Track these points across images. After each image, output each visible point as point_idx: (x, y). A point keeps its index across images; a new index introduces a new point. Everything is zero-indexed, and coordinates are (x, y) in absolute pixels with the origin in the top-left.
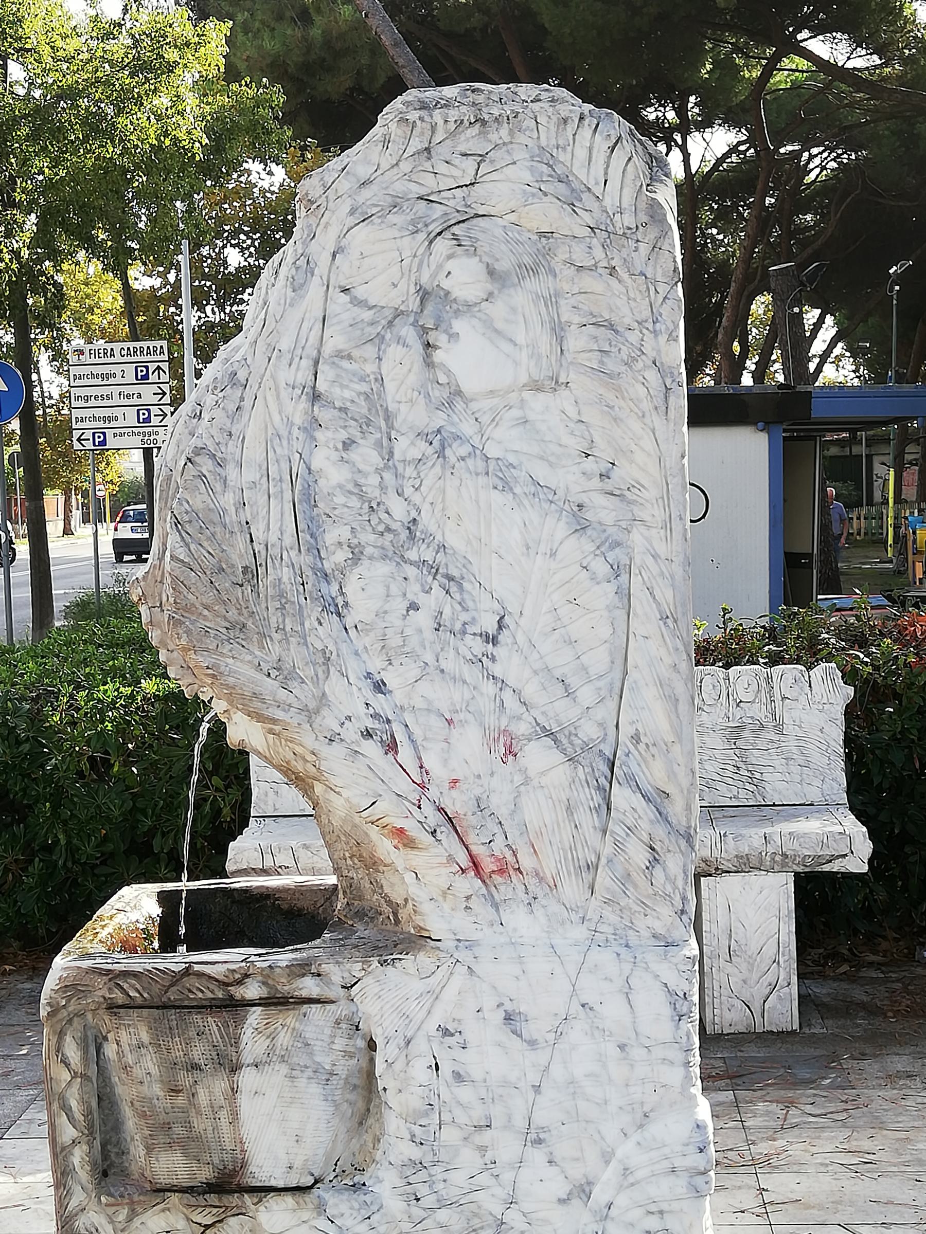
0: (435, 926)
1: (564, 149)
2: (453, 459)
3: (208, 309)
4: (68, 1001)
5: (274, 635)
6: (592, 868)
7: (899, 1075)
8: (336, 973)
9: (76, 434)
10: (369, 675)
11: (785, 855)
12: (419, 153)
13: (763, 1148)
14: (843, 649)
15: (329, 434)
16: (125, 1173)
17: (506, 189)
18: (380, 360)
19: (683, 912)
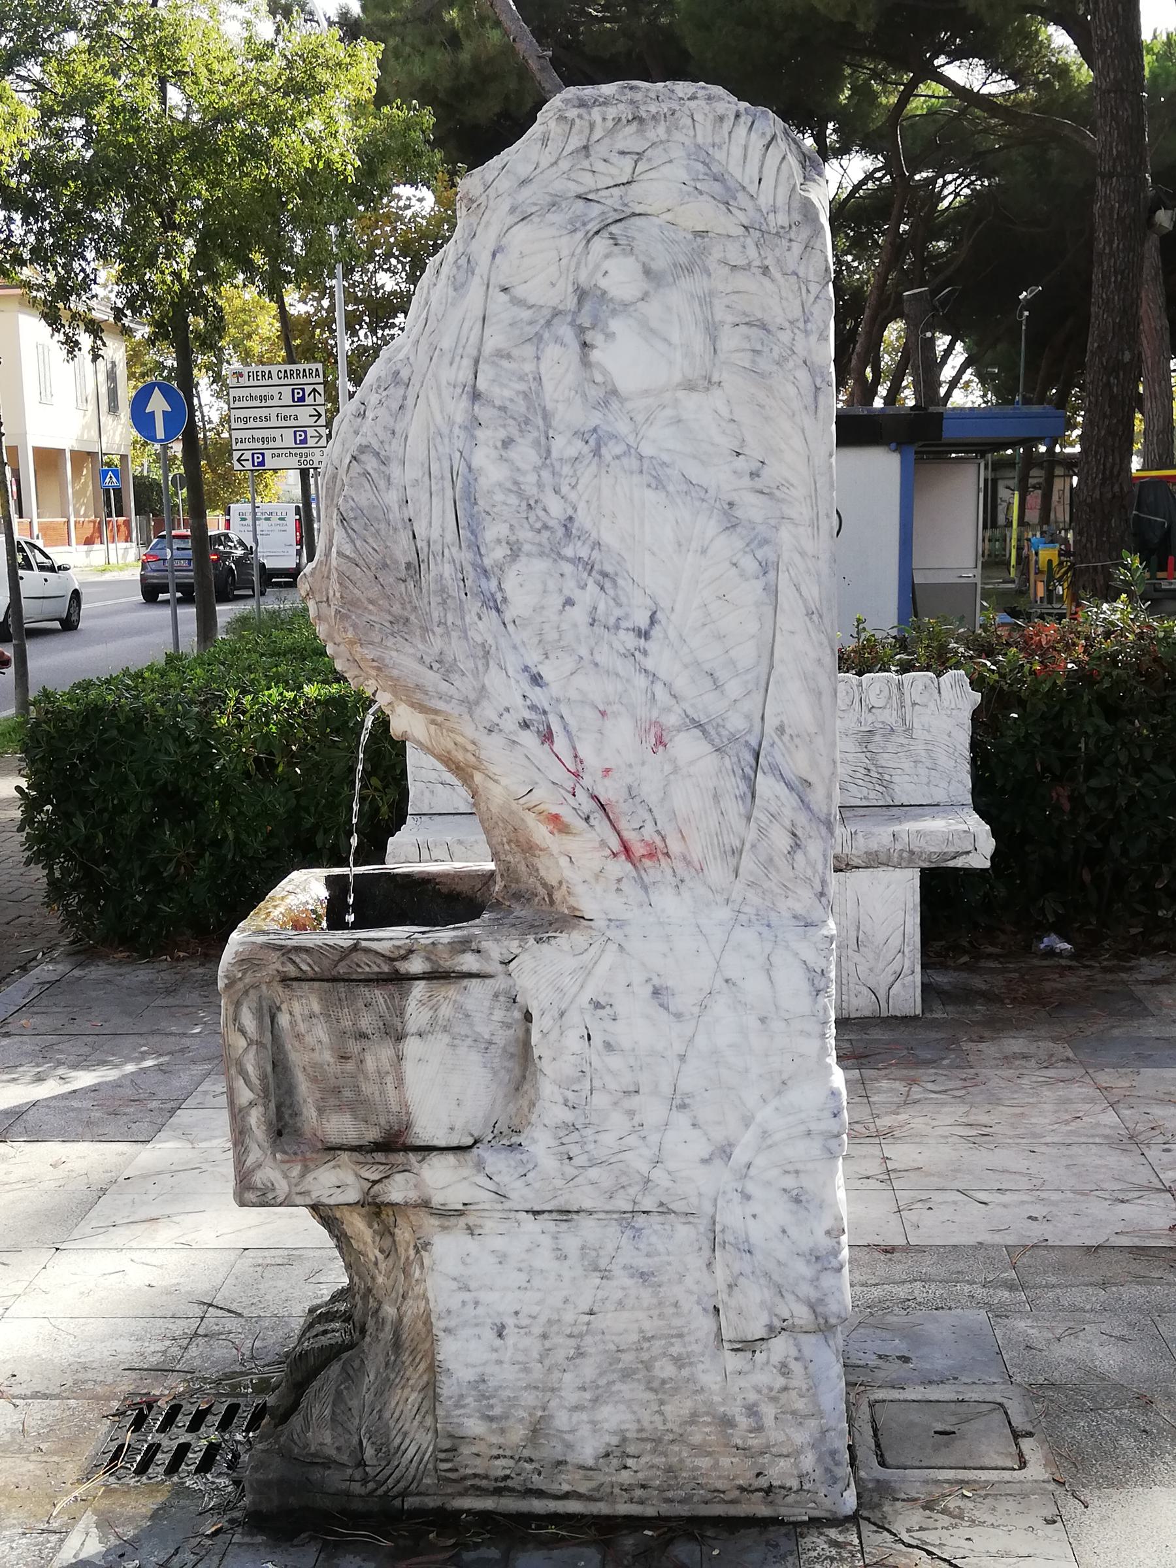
0: (588, 907)
1: (720, 147)
2: (608, 457)
3: (361, 333)
4: (244, 974)
5: (436, 629)
6: (737, 852)
7: (1015, 1056)
8: (495, 949)
9: (236, 455)
10: (526, 669)
11: (912, 853)
12: (577, 151)
13: (885, 1122)
14: (971, 657)
15: (489, 433)
16: (297, 1132)
17: (663, 188)
18: (538, 358)
19: (822, 894)
